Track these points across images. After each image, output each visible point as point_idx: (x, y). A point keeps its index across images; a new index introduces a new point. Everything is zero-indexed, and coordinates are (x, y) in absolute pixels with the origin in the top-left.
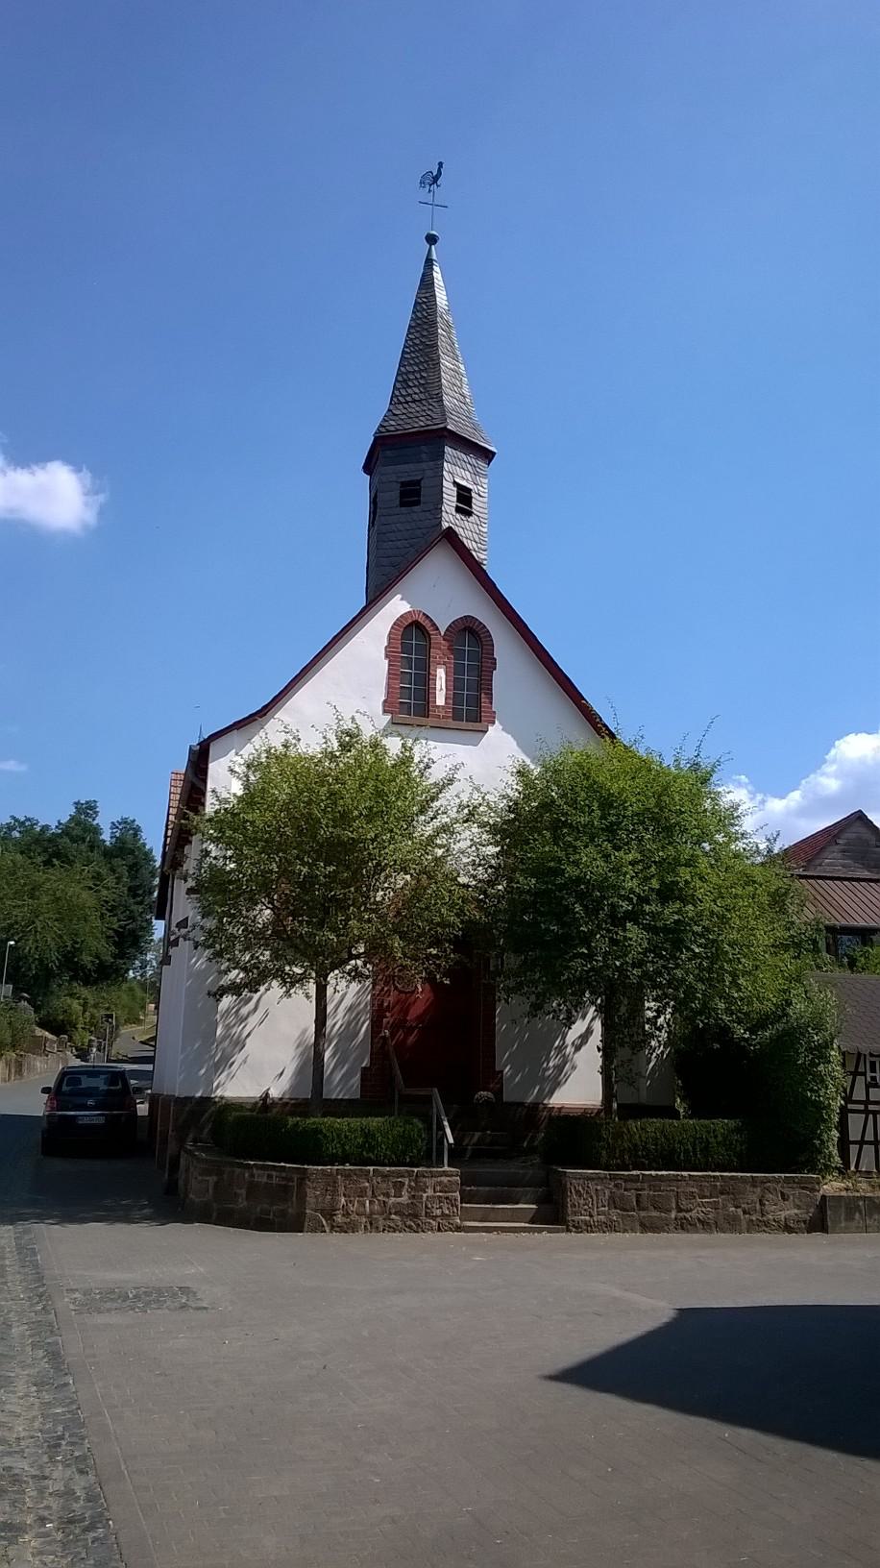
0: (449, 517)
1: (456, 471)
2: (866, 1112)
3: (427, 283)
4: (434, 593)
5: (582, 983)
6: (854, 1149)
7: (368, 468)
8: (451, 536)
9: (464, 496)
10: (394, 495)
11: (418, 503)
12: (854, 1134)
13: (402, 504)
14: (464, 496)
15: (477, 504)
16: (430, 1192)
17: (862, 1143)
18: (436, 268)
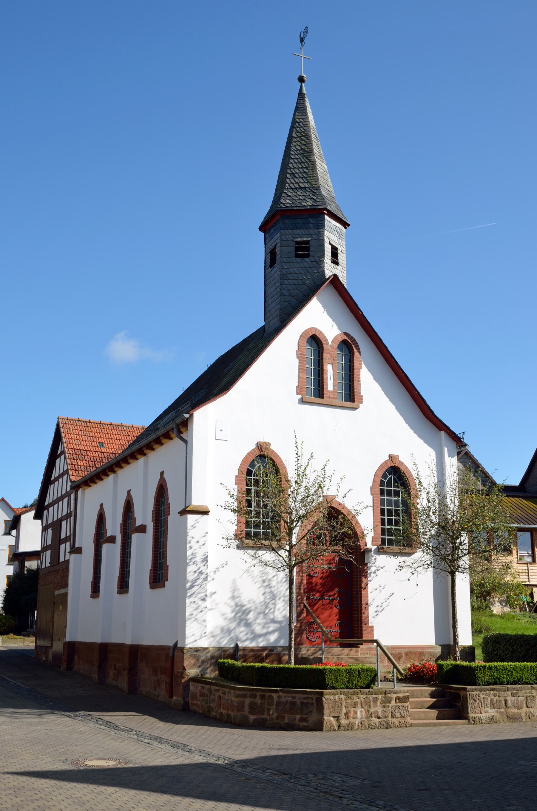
0: (329, 269)
1: (332, 234)
3: (300, 108)
4: (317, 316)
7: (263, 228)
8: (335, 281)
11: (308, 256)
13: (297, 256)
15: (342, 257)
16: (393, 703)
18: (307, 100)
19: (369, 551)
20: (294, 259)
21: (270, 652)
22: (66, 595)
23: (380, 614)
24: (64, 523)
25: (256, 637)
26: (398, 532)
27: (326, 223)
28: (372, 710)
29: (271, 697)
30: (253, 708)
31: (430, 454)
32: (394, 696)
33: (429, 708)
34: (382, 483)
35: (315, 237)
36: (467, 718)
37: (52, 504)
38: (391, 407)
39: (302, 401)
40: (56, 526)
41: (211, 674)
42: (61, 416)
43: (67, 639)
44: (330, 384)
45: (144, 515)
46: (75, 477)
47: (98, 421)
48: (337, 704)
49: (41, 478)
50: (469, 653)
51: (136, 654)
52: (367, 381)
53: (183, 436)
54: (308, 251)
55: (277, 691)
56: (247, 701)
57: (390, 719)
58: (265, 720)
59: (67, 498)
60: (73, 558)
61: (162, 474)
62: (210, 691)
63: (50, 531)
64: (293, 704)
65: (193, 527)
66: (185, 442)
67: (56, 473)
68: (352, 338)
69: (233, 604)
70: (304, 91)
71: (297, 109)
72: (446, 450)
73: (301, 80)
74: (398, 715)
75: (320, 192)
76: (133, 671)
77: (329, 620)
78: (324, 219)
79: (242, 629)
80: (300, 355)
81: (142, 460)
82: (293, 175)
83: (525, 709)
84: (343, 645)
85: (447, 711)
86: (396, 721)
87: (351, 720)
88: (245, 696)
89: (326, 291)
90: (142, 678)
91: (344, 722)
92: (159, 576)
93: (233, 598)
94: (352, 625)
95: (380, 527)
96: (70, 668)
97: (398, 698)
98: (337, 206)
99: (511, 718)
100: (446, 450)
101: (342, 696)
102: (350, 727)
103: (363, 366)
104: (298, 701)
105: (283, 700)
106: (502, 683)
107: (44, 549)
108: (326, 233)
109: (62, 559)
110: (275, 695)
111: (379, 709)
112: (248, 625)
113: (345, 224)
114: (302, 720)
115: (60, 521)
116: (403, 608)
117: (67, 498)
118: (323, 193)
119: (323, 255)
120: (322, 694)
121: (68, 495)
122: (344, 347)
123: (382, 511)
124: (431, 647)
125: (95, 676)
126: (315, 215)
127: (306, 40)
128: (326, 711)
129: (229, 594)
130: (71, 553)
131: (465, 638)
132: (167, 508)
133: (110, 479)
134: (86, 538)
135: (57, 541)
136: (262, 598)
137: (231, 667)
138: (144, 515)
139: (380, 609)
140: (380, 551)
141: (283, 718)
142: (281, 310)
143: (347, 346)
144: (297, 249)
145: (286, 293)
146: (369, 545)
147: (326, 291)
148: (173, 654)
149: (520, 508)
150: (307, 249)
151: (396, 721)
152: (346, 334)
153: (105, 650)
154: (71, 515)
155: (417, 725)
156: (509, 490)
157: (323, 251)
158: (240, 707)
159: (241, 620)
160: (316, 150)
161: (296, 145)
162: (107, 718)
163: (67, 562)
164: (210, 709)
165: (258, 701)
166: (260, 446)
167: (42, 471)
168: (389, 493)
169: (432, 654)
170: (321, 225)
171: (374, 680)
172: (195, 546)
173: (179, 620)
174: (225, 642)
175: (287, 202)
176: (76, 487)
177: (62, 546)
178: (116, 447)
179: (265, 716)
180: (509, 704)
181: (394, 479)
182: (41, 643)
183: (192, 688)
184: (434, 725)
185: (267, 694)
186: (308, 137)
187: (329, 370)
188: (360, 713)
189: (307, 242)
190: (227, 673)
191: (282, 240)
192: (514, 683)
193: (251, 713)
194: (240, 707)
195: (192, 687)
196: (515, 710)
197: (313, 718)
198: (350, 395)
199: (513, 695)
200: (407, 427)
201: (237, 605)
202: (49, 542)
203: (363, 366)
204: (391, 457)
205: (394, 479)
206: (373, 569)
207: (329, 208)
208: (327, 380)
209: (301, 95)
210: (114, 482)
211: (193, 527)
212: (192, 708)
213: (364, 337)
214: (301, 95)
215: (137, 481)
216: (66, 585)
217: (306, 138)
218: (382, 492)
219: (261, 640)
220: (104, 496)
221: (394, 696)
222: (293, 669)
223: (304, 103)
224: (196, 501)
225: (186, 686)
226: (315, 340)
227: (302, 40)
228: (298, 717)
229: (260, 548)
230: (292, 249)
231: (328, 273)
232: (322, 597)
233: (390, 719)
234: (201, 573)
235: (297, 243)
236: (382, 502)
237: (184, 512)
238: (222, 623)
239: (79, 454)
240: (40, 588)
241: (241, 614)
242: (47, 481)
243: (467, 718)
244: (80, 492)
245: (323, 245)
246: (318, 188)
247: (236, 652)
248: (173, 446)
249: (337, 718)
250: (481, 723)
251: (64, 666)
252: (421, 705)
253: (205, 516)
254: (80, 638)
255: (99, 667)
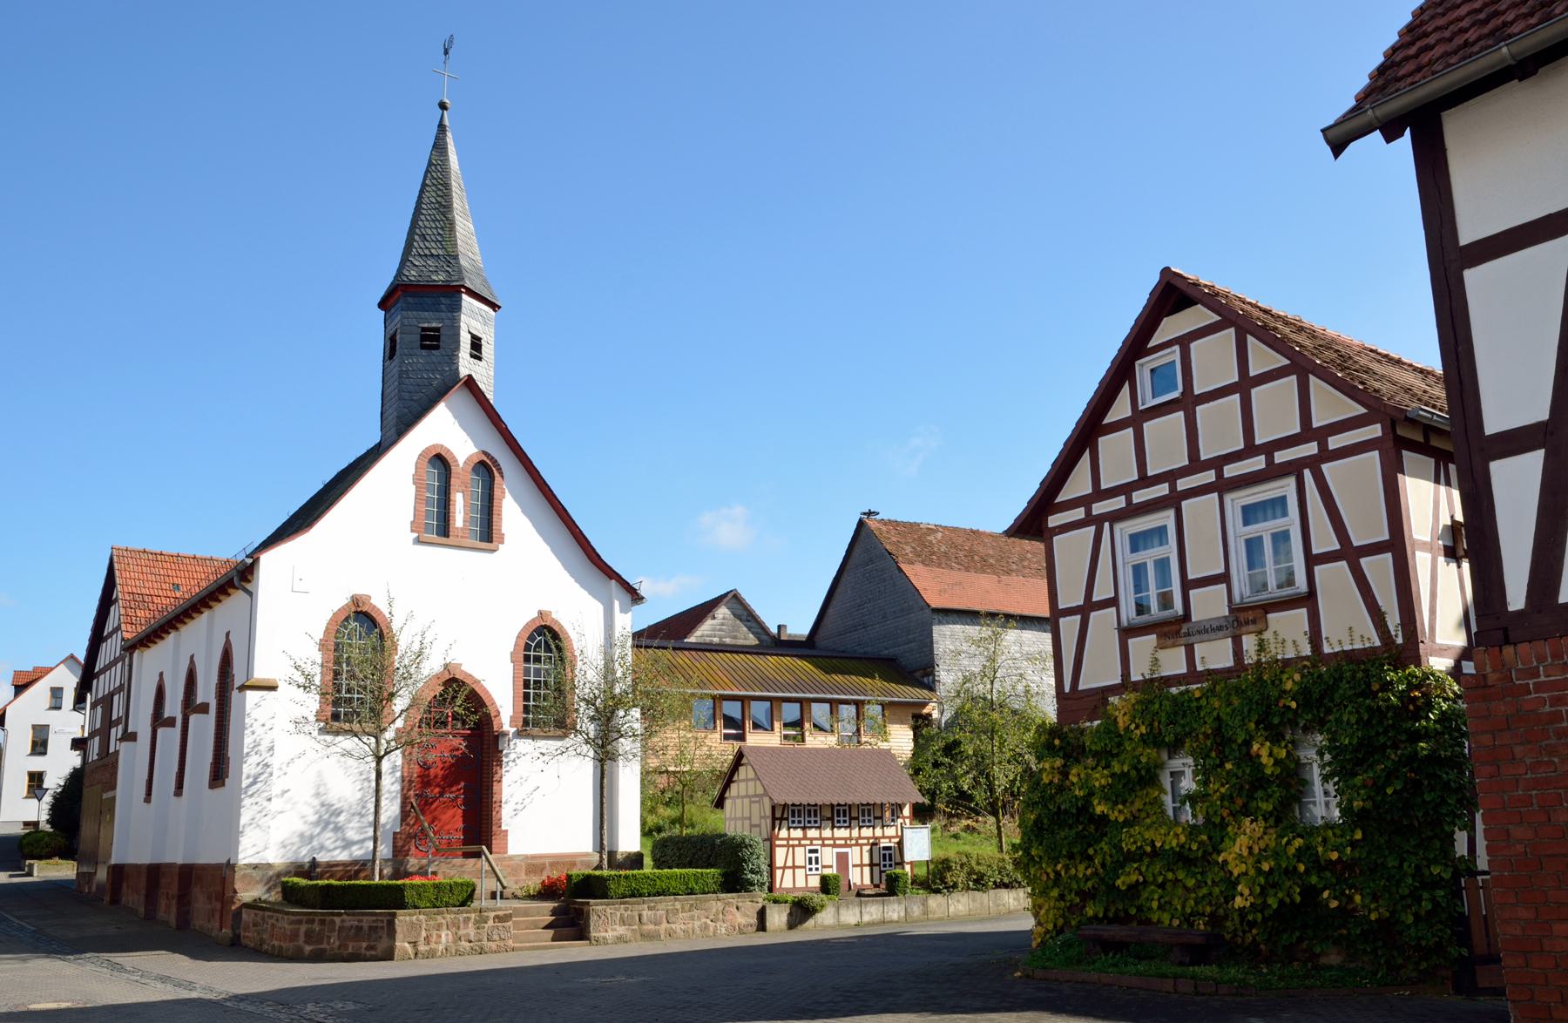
0: (465, 365)
1: (472, 318)
2: (788, 846)
3: (439, 146)
4: (444, 428)
5: (1206, 783)
6: (779, 873)
7: (384, 304)
8: (470, 383)
9: (476, 344)
10: (410, 339)
11: (437, 347)
12: (779, 862)
13: (423, 347)
14: (476, 344)
15: (487, 350)
16: (491, 923)
17: (784, 868)
18: (449, 134)
19: (505, 734)
20: (419, 351)
21: (360, 867)
22: (114, 799)
23: (520, 814)
24: (116, 698)
25: (348, 844)
26: (547, 708)
27: (464, 304)
28: (462, 932)
29: (333, 922)
30: (309, 937)
31: (597, 608)
32: (492, 915)
33: (546, 927)
34: (527, 647)
35: (447, 322)
36: (588, 939)
37: (103, 671)
38: (545, 550)
39: (418, 541)
40: (106, 702)
41: (275, 896)
42: (117, 545)
43: (113, 861)
44: (459, 518)
45: (206, 692)
46: (129, 633)
47: (174, 552)
48: (414, 927)
49: (88, 633)
50: (635, 860)
51: (189, 875)
52: (513, 514)
53: (248, 586)
54: (438, 342)
55: (340, 915)
56: (303, 928)
57: (485, 942)
58: (324, 951)
59: (1363, 410)
60: (124, 747)
61: (228, 634)
62: (263, 918)
63: (99, 709)
64: (359, 929)
65: (257, 705)
66: (250, 594)
67: (109, 628)
68: (492, 459)
69: (316, 802)
70: (446, 122)
71: (435, 146)
72: (617, 604)
73: (443, 106)
74: (496, 937)
75: (458, 263)
76: (184, 899)
77: (453, 820)
78: (460, 299)
79: (330, 834)
80: (417, 480)
81: (206, 614)
82: (423, 237)
83: (665, 925)
84: (467, 855)
85: (565, 931)
86: (493, 945)
87: (433, 946)
88: (300, 922)
89: (458, 395)
90: (185, 905)
91: (422, 948)
92: (220, 772)
93: (317, 795)
94: (480, 828)
95: (522, 703)
96: (115, 901)
97: (497, 917)
98: (485, 281)
99: (646, 936)
100: (617, 604)
101: (422, 917)
102: (431, 954)
103: (507, 494)
104: (365, 925)
105: (347, 924)
106: (641, 895)
107: (92, 735)
108: (463, 317)
109: (112, 750)
110: (337, 920)
111: (471, 931)
112: (337, 829)
113: (494, 306)
114: (369, 948)
115: (112, 695)
116: (549, 805)
117: (1363, 410)
118: (462, 262)
119: (458, 348)
120: (394, 915)
121: (120, 659)
122: (482, 469)
123: (526, 684)
124: (587, 854)
125: (142, 910)
126: (449, 294)
127: (451, 52)
128: (399, 936)
129: (301, 795)
130: (121, 740)
131: (629, 840)
132: (230, 679)
133: (171, 638)
134: (141, 721)
135: (108, 723)
136: (359, 795)
137: (295, 887)
138: (206, 692)
139: (520, 807)
140: (520, 734)
141: (346, 947)
142: (401, 416)
143: (485, 469)
144: (423, 338)
145: (406, 396)
146: (506, 727)
147: (458, 395)
148: (221, 875)
149: (789, 670)
150: (437, 338)
151: (493, 945)
152: (485, 453)
153: (155, 872)
154: (125, 688)
155: (521, 949)
156: (777, 644)
157: (457, 342)
158: (294, 936)
159: (327, 823)
160: (457, 204)
161: (430, 195)
162: (118, 960)
163: (117, 752)
164: (262, 942)
165: (316, 927)
166: (356, 600)
167: (90, 623)
168: (537, 659)
169: (587, 865)
170: (456, 307)
171: (470, 897)
172: (260, 731)
173: (231, 831)
174: (304, 855)
175: (412, 274)
176: (131, 647)
177: (113, 731)
178: (191, 587)
179: (324, 946)
180: (645, 919)
181: (544, 642)
182: (85, 869)
183: (244, 916)
184: (552, 947)
185: (328, 918)
186: (447, 186)
187: (459, 501)
188: (446, 936)
189: (437, 329)
190: (291, 894)
191: (403, 325)
192: (659, 894)
193: (306, 942)
194: (294, 936)
195: (246, 916)
196: (652, 927)
197: (382, 946)
198: (487, 532)
199: (650, 908)
200: (566, 574)
201: (323, 805)
202: (98, 726)
203: (507, 494)
204: (540, 613)
205: (544, 642)
206: (512, 756)
207: (468, 284)
208: (454, 510)
209: (442, 128)
210: (160, 643)
211: (257, 705)
212: (244, 941)
213: (507, 458)
214: (442, 128)
215: (197, 641)
216: (113, 787)
217: (444, 187)
218: (527, 659)
219: (354, 848)
220: (156, 663)
221: (492, 915)
222: (377, 886)
223: (444, 139)
224: (260, 673)
225: (238, 914)
226: (440, 461)
227: (446, 52)
228: (364, 945)
229: (337, 733)
230: (418, 337)
231: (463, 372)
232: (441, 794)
233: (485, 942)
234: (267, 765)
235: (424, 329)
236: (527, 671)
237: (243, 688)
238: (300, 827)
239: (139, 600)
240: (85, 791)
241: (329, 818)
242: (98, 637)
243: (588, 939)
244: (135, 655)
245: (458, 335)
246: (456, 257)
247: (311, 869)
248: (238, 597)
249: (414, 944)
250: (606, 944)
251: (107, 898)
252: (535, 925)
253: (272, 693)
254: (131, 859)
255: (147, 896)
